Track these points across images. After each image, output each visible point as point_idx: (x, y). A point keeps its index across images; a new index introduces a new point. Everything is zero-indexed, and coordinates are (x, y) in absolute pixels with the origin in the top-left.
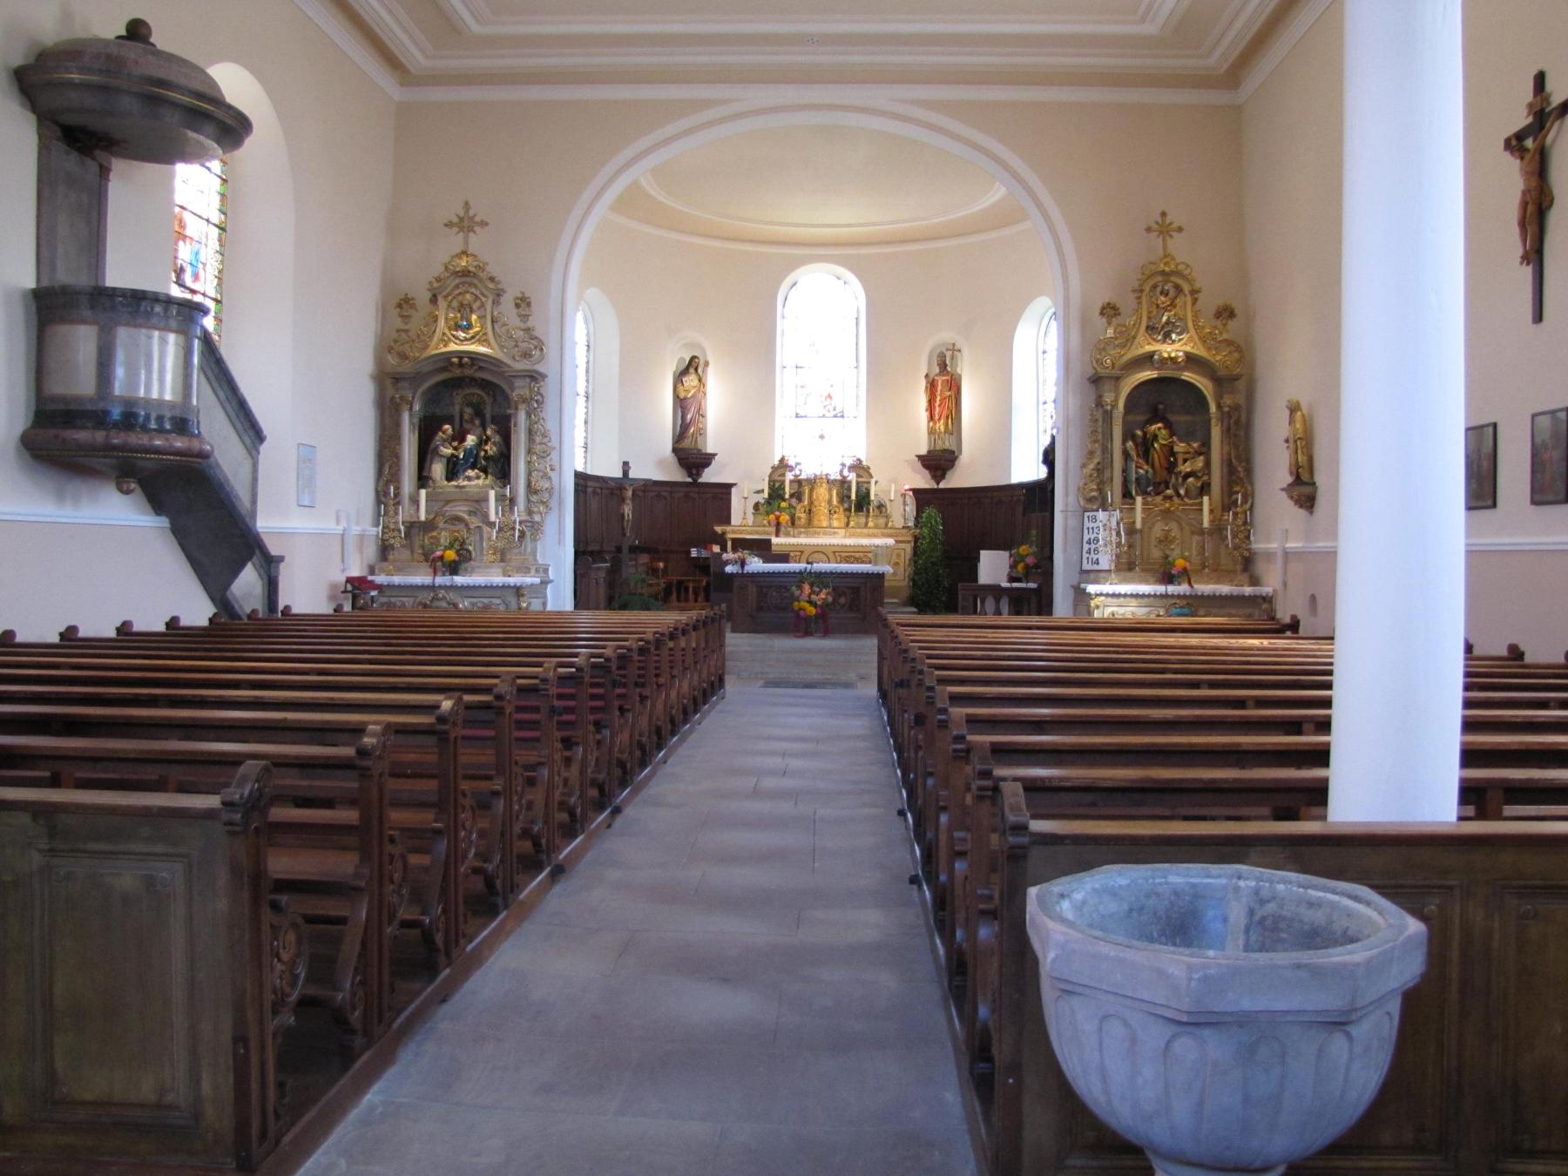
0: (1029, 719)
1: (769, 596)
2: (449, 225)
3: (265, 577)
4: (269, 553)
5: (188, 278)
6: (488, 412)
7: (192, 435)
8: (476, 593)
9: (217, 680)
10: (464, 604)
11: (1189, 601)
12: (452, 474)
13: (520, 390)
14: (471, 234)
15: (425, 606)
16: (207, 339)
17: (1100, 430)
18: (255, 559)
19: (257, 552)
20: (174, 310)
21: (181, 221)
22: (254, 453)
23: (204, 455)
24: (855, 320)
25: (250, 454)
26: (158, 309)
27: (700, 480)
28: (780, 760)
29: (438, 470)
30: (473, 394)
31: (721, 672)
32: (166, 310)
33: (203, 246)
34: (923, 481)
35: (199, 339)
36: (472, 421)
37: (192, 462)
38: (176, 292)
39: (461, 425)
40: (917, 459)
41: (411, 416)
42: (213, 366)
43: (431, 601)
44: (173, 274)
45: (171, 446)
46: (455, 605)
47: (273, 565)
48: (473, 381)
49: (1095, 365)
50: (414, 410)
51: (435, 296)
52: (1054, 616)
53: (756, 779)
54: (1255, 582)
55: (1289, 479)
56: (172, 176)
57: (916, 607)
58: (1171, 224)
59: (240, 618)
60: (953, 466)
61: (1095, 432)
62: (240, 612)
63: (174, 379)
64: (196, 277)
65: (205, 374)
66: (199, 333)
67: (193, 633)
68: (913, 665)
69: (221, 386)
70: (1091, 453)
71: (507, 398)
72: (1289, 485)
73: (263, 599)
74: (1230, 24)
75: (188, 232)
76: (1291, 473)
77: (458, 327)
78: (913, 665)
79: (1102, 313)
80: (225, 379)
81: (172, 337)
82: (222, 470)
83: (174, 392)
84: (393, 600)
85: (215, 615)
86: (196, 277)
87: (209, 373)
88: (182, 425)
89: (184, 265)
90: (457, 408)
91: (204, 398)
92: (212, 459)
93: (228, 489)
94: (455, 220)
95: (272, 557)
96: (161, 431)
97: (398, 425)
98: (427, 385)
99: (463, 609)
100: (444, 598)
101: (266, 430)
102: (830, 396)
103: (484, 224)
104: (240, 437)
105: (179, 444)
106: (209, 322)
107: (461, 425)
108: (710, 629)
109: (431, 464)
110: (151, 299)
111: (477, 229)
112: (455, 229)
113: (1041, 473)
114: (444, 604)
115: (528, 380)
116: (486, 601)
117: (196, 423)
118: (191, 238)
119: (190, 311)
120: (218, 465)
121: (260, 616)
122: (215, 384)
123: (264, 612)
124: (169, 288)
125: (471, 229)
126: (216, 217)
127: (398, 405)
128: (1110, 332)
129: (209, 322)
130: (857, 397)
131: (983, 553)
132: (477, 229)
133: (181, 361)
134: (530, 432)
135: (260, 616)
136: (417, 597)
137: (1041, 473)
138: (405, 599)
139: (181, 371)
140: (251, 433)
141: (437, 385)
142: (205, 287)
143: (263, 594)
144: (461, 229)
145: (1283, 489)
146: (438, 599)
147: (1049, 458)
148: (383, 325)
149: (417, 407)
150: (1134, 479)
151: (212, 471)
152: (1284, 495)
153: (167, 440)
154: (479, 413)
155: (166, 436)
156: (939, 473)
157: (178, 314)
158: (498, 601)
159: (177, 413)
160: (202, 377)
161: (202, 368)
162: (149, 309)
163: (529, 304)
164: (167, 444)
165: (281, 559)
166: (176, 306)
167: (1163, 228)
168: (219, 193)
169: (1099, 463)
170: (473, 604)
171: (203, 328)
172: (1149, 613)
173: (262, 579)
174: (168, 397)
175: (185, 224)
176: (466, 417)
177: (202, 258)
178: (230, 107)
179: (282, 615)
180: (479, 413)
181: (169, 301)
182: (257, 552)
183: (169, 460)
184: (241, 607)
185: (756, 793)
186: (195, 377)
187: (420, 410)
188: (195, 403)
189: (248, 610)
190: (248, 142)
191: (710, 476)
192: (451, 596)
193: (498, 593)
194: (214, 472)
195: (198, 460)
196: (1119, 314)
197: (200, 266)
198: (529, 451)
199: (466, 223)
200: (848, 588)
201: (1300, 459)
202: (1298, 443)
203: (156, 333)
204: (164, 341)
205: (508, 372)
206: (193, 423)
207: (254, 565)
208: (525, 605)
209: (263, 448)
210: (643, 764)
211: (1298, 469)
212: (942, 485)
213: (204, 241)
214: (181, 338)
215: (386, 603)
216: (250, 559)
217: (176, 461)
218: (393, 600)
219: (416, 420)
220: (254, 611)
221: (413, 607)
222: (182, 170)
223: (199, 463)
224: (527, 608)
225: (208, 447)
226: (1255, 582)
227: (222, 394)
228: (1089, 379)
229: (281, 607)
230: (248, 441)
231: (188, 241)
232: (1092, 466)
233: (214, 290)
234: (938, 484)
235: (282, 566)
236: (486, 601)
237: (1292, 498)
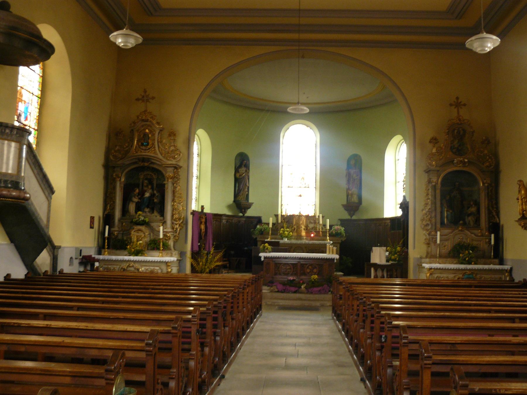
0: (449, 342)
1: (280, 268)
2: (138, 100)
3: (52, 255)
4: (54, 244)
5: (22, 119)
6: (155, 182)
7: (21, 189)
8: (147, 264)
9: (25, 312)
10: (142, 269)
11: (472, 272)
12: (138, 208)
13: (170, 173)
14: (148, 103)
15: (124, 270)
16: (29, 146)
17: (430, 194)
18: (47, 247)
19: (49, 244)
20: (15, 132)
21: (20, 93)
22: (49, 198)
23: (27, 199)
24: (315, 145)
25: (47, 198)
26: (7, 131)
27: (246, 215)
28: (294, 348)
29: (132, 207)
30: (148, 174)
31: (260, 303)
32: (11, 131)
33: (30, 105)
34: (346, 216)
35: (26, 145)
36: (147, 186)
37: (20, 202)
38: (16, 124)
39: (142, 188)
40: (342, 206)
41: (120, 183)
42: (32, 158)
43: (127, 267)
44: (16, 117)
45: (11, 195)
46: (138, 270)
47: (56, 250)
48: (148, 168)
49: (428, 164)
50: (121, 181)
51: (132, 130)
52: (409, 279)
53: (285, 359)
54: (501, 263)
55: (519, 217)
56: (17, 73)
57: (342, 272)
58: (460, 102)
59: (40, 275)
60: (358, 209)
61: (428, 194)
62: (40, 272)
63: (13, 164)
64: (26, 119)
65: (29, 164)
66: (26, 143)
67: (17, 281)
68: (365, 308)
69: (35, 167)
70: (427, 204)
71: (163, 176)
72: (519, 219)
73: (51, 265)
74: (259, 109)
75: (23, 98)
76: (520, 214)
77: (142, 145)
78: (365, 308)
79: (430, 142)
80: (37, 164)
81: (13, 144)
82: (34, 207)
83: (13, 169)
84: (110, 266)
85: (28, 273)
86: (26, 119)
87: (30, 161)
88: (16, 185)
89: (21, 113)
90: (141, 180)
91: (27, 172)
92: (29, 201)
93: (37, 215)
94: (140, 97)
95: (55, 246)
96: (6, 187)
97: (114, 188)
98: (127, 170)
99: (141, 272)
100: (133, 266)
101: (55, 189)
102: (303, 178)
103: (153, 98)
104: (43, 191)
105: (14, 194)
106: (32, 139)
107: (142, 188)
108: (256, 283)
109: (129, 205)
110: (4, 126)
111: (150, 100)
112: (141, 101)
113: (399, 213)
114: (132, 269)
115: (173, 168)
116: (152, 268)
117: (23, 184)
118: (25, 102)
119: (23, 132)
120: (32, 204)
121: (49, 273)
122: (33, 167)
123: (50, 272)
124: (14, 122)
125: (147, 101)
126: (39, 93)
127: (115, 178)
128: (434, 150)
129: (32, 139)
130: (282, 179)
131: (374, 248)
132: (150, 100)
133: (17, 156)
134: (174, 192)
135: (49, 273)
136: (121, 265)
137: (399, 213)
138: (115, 266)
139: (17, 160)
140: (48, 189)
141: (131, 170)
142: (31, 123)
143: (51, 262)
144: (143, 101)
145: (516, 221)
146: (130, 267)
147: (404, 206)
148: (109, 143)
149: (123, 180)
150: (446, 216)
151: (30, 206)
152: (517, 224)
153: (9, 191)
154: (151, 182)
155: (8, 189)
156: (352, 212)
157: (17, 133)
158: (157, 268)
159: (14, 179)
160: (28, 166)
161: (27, 159)
162: (3, 131)
163: (175, 135)
164: (9, 194)
165: (60, 247)
166: (16, 129)
167: (458, 104)
168: (39, 82)
169: (430, 209)
170: (147, 269)
171: (28, 141)
172: (455, 277)
173: (50, 256)
174: (10, 172)
175: (22, 95)
176: (145, 185)
177: (29, 110)
178: (45, 41)
179: (59, 273)
180: (151, 182)
181: (13, 127)
182: (49, 244)
183: (9, 201)
184: (40, 269)
185: (287, 367)
186: (23, 163)
187: (124, 181)
188: (23, 175)
189: (43, 271)
190: (52, 57)
191: (250, 213)
192: (137, 265)
193: (158, 264)
194: (31, 207)
195: (23, 201)
196: (438, 142)
197: (28, 114)
198: (173, 200)
199: (145, 98)
200: (318, 265)
201: (524, 207)
202: (523, 200)
203: (6, 142)
204: (9, 146)
205: (164, 164)
206: (22, 183)
207: (47, 250)
208: (170, 270)
209: (53, 196)
210: (232, 351)
211: (523, 212)
212: (354, 217)
213: (30, 103)
214: (18, 144)
215: (106, 268)
216: (45, 247)
217: (12, 201)
218: (110, 266)
219: (122, 185)
220: (46, 271)
221: (118, 270)
222: (23, 70)
223: (24, 203)
224: (171, 272)
225: (28, 195)
226: (501, 263)
227: (35, 171)
228: (425, 171)
229: (59, 270)
230: (47, 193)
231: (23, 102)
232: (427, 210)
233: (34, 125)
234: (351, 217)
235: (60, 250)
236: (152, 268)
237: (520, 225)
